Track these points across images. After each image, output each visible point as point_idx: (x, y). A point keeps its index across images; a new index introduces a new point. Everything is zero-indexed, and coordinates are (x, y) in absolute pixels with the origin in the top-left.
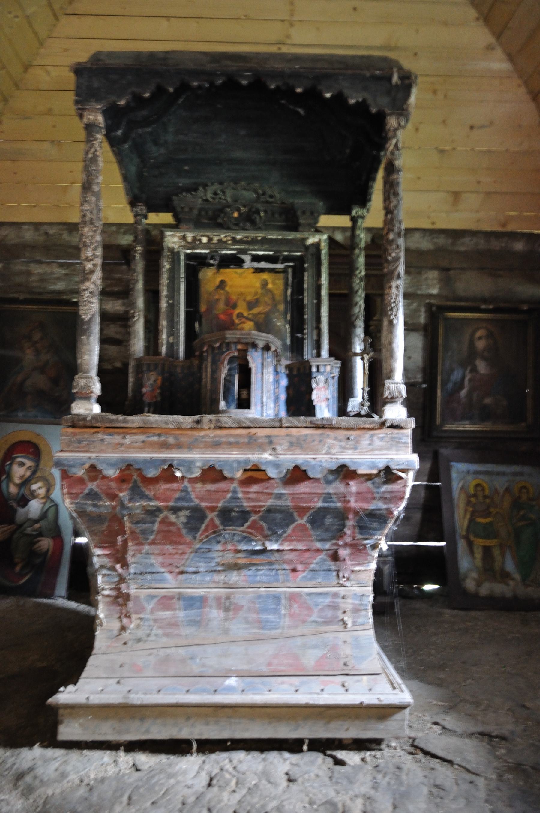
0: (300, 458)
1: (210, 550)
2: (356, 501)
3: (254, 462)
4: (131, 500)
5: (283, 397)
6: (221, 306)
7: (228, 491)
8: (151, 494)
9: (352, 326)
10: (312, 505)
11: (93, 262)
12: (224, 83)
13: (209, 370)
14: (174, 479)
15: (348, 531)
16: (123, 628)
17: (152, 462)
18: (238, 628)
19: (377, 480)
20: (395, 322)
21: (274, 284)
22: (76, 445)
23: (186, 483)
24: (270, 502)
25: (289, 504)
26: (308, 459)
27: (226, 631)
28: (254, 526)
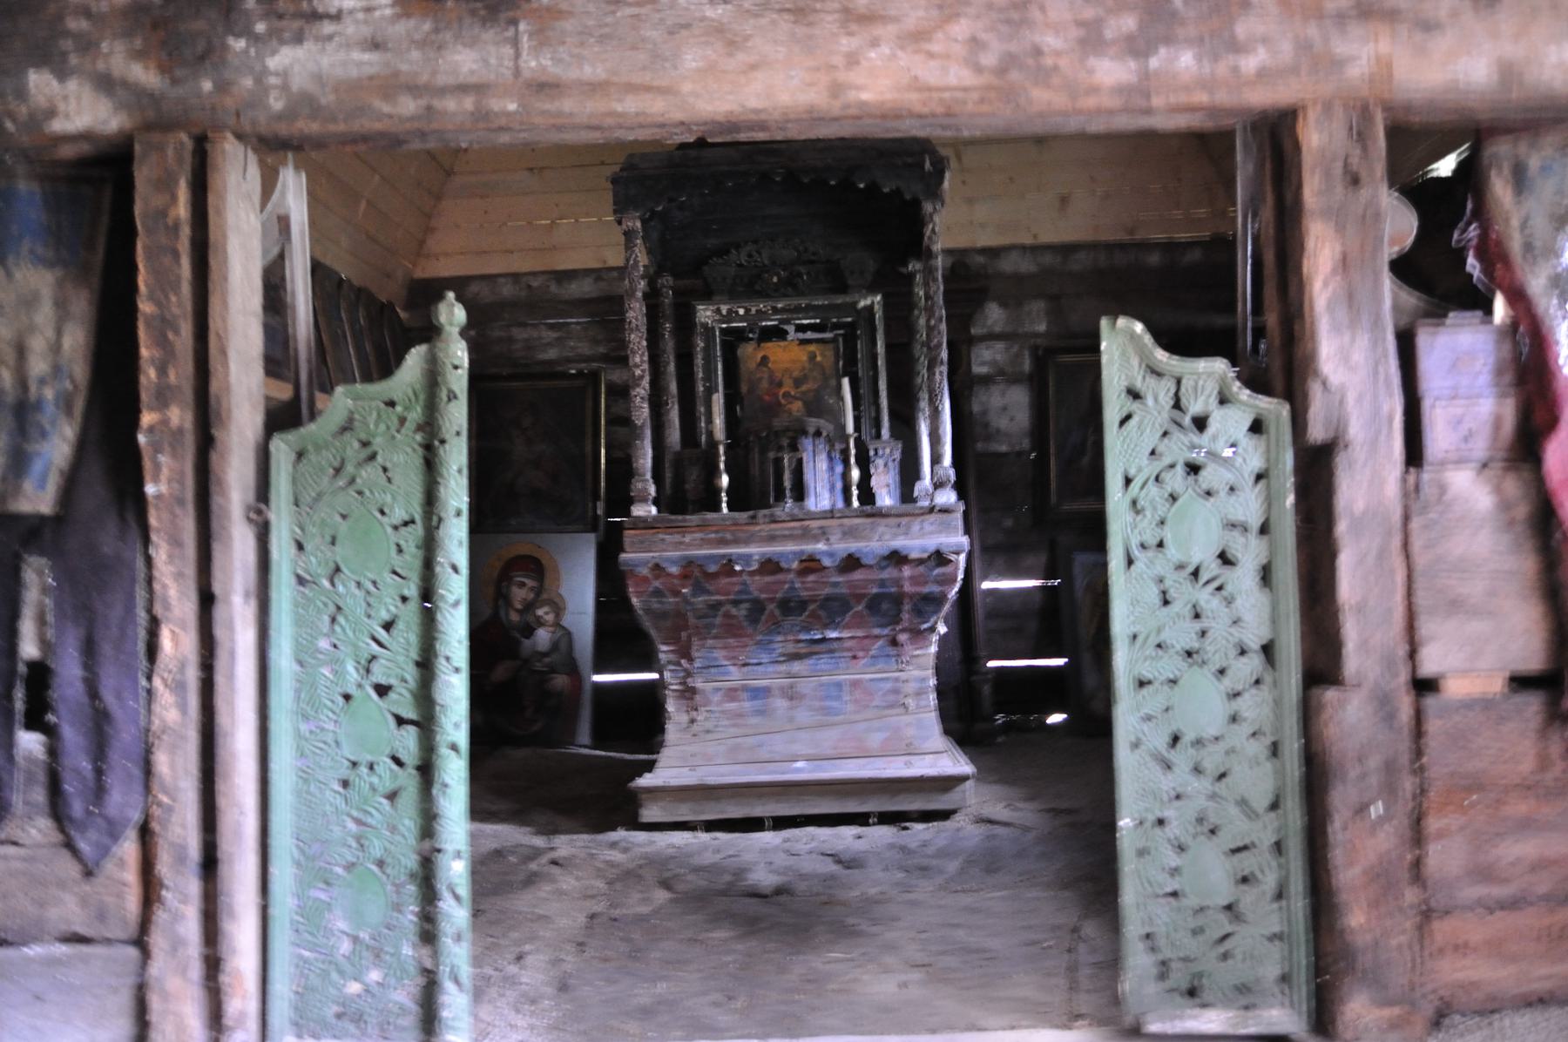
0: (853, 546)
1: (771, 642)
6: (765, 384)
14: (733, 573)
15: (905, 616)
16: (693, 721)
18: (803, 716)
21: (822, 355)
23: (745, 577)
24: (827, 591)
27: (791, 719)
28: (813, 615)
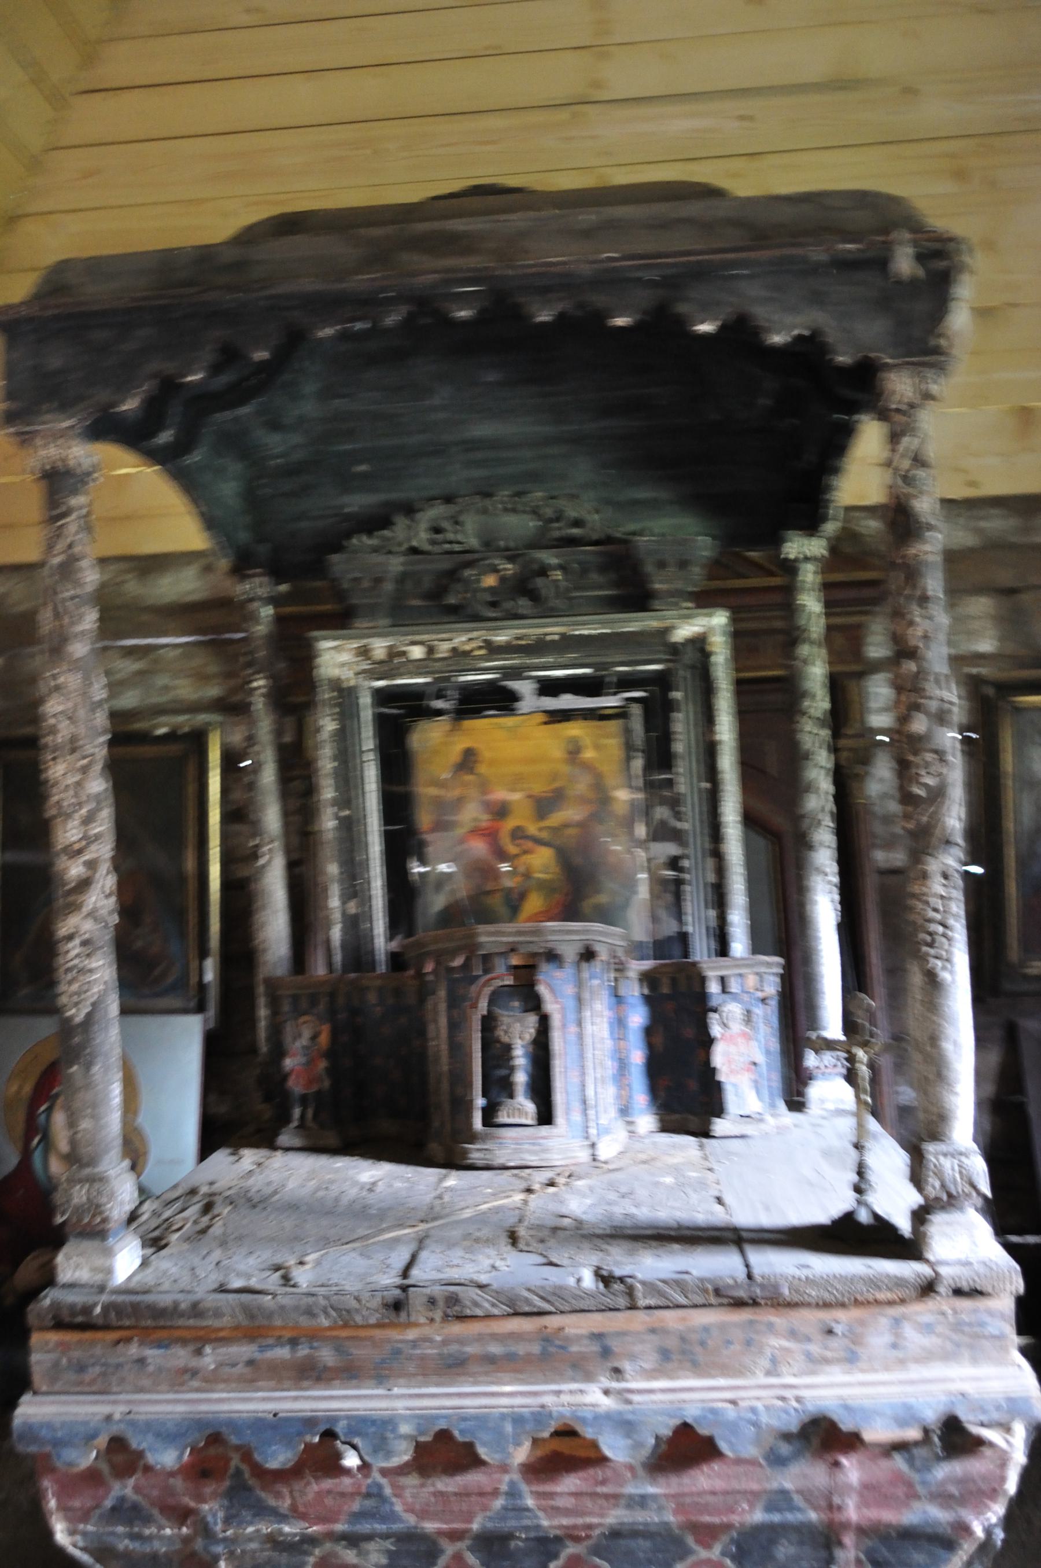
2: (858, 1508)
3: (561, 1415)
4: (227, 1521)
5: (637, 1057)
7: (495, 1493)
8: (285, 1504)
9: (803, 843)
10: (735, 1519)
11: (87, 857)
12: (409, 322)
13: (443, 1021)
17: (277, 1426)
19: (920, 1452)
20: (945, 976)
21: (597, 747)
22: (72, 1376)
24: (615, 1516)
25: (670, 1518)
26: (720, 1405)
